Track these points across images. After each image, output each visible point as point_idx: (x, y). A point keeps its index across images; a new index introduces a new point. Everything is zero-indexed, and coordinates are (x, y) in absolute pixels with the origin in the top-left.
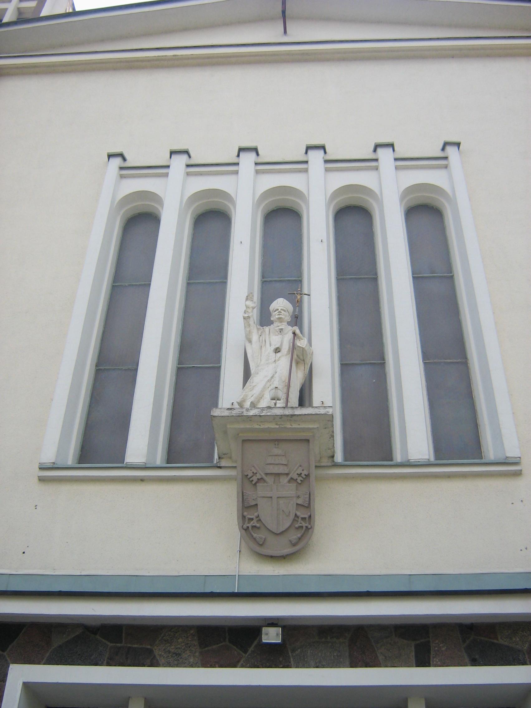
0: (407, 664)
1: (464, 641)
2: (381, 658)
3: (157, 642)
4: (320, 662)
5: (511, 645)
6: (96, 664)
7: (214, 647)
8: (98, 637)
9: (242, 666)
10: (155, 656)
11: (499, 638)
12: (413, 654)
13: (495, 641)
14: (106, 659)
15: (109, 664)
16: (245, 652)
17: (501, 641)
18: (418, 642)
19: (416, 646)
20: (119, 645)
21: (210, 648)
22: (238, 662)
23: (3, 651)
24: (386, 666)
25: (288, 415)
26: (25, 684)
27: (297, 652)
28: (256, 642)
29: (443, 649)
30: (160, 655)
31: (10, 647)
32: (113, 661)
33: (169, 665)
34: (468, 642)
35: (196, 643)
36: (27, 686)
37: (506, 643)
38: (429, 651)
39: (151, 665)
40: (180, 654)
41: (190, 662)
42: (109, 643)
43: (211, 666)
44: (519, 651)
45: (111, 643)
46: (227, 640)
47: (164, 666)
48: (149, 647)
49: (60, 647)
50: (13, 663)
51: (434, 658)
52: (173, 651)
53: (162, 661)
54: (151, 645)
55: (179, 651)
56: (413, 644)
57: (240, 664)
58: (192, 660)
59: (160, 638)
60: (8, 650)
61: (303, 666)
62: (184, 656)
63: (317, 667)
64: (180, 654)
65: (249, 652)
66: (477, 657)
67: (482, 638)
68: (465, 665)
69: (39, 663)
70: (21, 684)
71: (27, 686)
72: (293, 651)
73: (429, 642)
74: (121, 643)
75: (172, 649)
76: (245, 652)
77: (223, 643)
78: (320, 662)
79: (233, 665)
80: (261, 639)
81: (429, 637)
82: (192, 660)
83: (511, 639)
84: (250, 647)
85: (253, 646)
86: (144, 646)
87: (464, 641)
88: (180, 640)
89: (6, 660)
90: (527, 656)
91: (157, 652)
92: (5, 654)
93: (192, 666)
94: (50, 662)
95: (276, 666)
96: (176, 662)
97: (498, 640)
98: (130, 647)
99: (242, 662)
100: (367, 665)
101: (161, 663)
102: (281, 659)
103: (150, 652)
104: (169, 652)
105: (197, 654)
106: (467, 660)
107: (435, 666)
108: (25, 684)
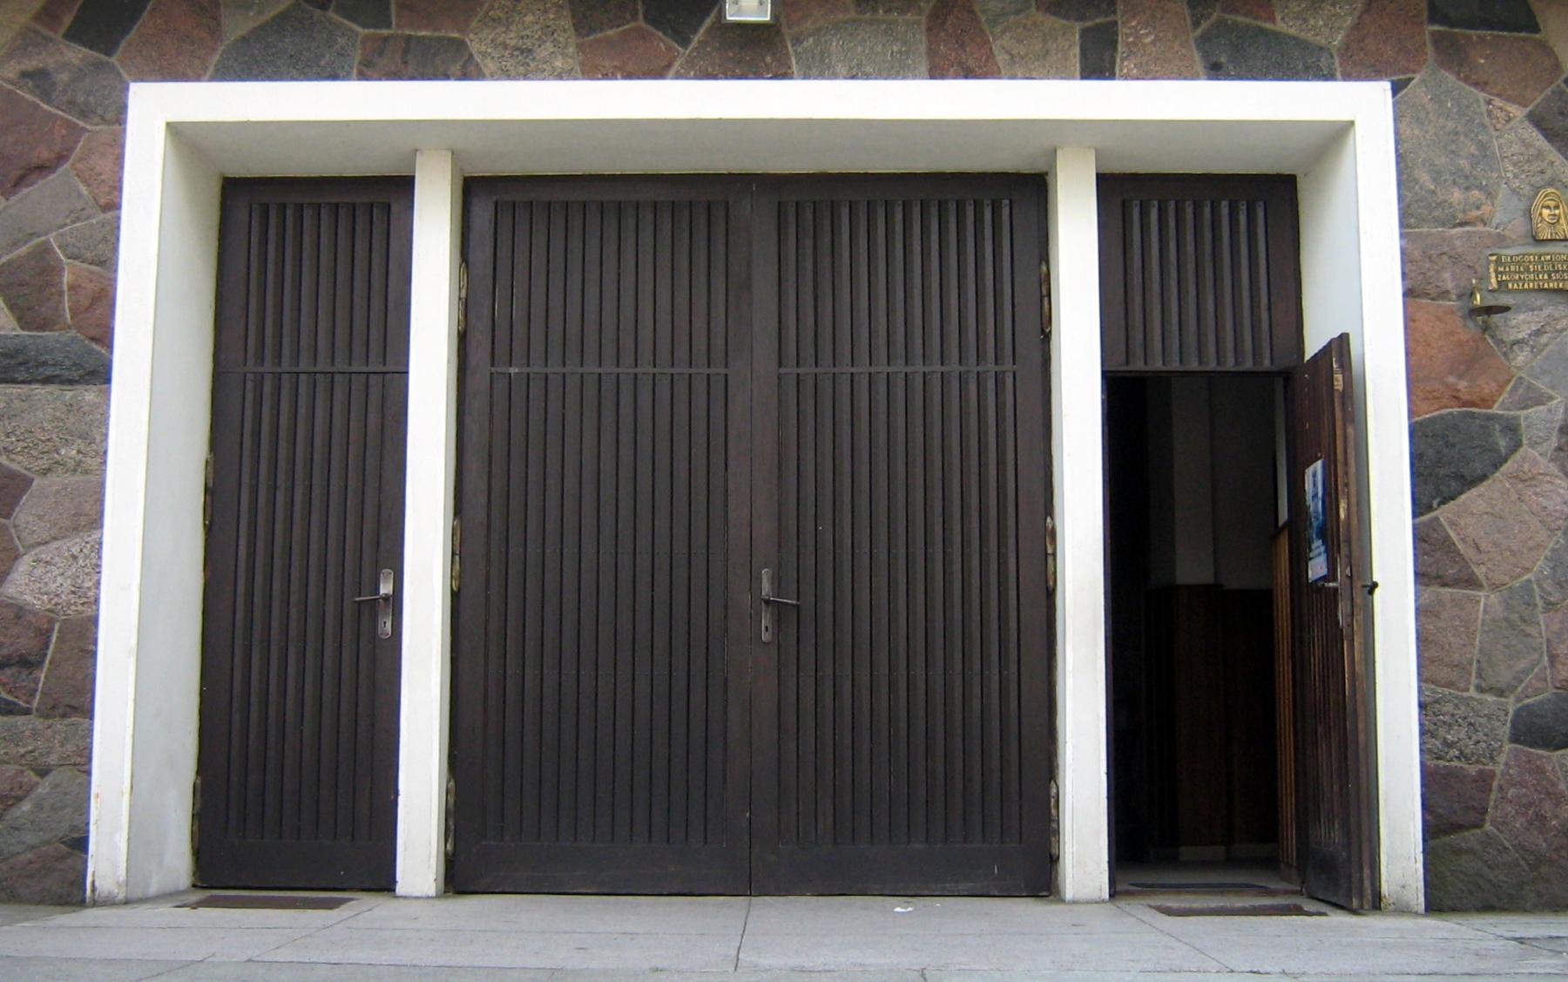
0: (1062, 74)
1: (1196, 24)
2: (1001, 58)
3: (474, 24)
4: (859, 66)
5: (1303, 35)
6: (334, 77)
7: (610, 32)
8: (331, 14)
9: (678, 76)
10: (471, 55)
11: (1278, 18)
12: (1077, 50)
13: (1269, 26)
14: (356, 63)
15: (363, 76)
16: (685, 42)
17: (1280, 26)
18: (1089, 24)
19: (1085, 33)
20: (385, 32)
21: (599, 35)
22: (669, 66)
23: (109, 53)
24: (1013, 77)
25: (47, 381)
26: (168, 124)
27: (805, 44)
28: (708, 22)
29: (1148, 40)
30: (484, 54)
31: (123, 44)
32: (382, 63)
33: (506, 75)
34: (1204, 25)
35: (567, 23)
36: (175, 131)
37: (1292, 31)
38: (1113, 44)
39: (465, 76)
40: (530, 51)
41: (554, 69)
42: (359, 29)
43: (605, 77)
44: (1321, 49)
45: (364, 26)
46: (641, 16)
47: (493, 77)
48: (456, 35)
49: (244, 39)
50: (135, 81)
51: (1123, 60)
52: (513, 43)
53: (490, 66)
54: (460, 31)
55: (528, 43)
56: (1078, 27)
57: (672, 71)
58: (558, 64)
59: (481, 14)
60: (120, 49)
61: (821, 76)
62: (542, 53)
63: (853, 77)
64: (530, 51)
65: (694, 43)
66: (1223, 60)
67: (1240, 19)
68: (1195, 77)
69: (198, 79)
70: (163, 127)
71: (175, 131)
72: (797, 41)
73: (1115, 23)
74: (389, 26)
75: (512, 39)
76: (685, 42)
77: (632, 25)
78: (859, 66)
79: (657, 71)
80: (722, 12)
81: (1114, 12)
82: (558, 64)
83: (1305, 20)
84: (695, 31)
85: (702, 31)
86: (442, 33)
87: (1196, 24)
88: (529, 18)
89: (119, 74)
90: (1337, 61)
91: (475, 46)
92: (114, 60)
93: (560, 77)
94: (224, 73)
95: (758, 76)
96: (522, 69)
97: (1273, 20)
98: (409, 38)
99: (676, 66)
100: (968, 74)
101: (486, 71)
102: (768, 59)
103: (460, 45)
104: (505, 46)
105: (571, 50)
106: (1199, 66)
107: (1126, 77)
108: (168, 124)
